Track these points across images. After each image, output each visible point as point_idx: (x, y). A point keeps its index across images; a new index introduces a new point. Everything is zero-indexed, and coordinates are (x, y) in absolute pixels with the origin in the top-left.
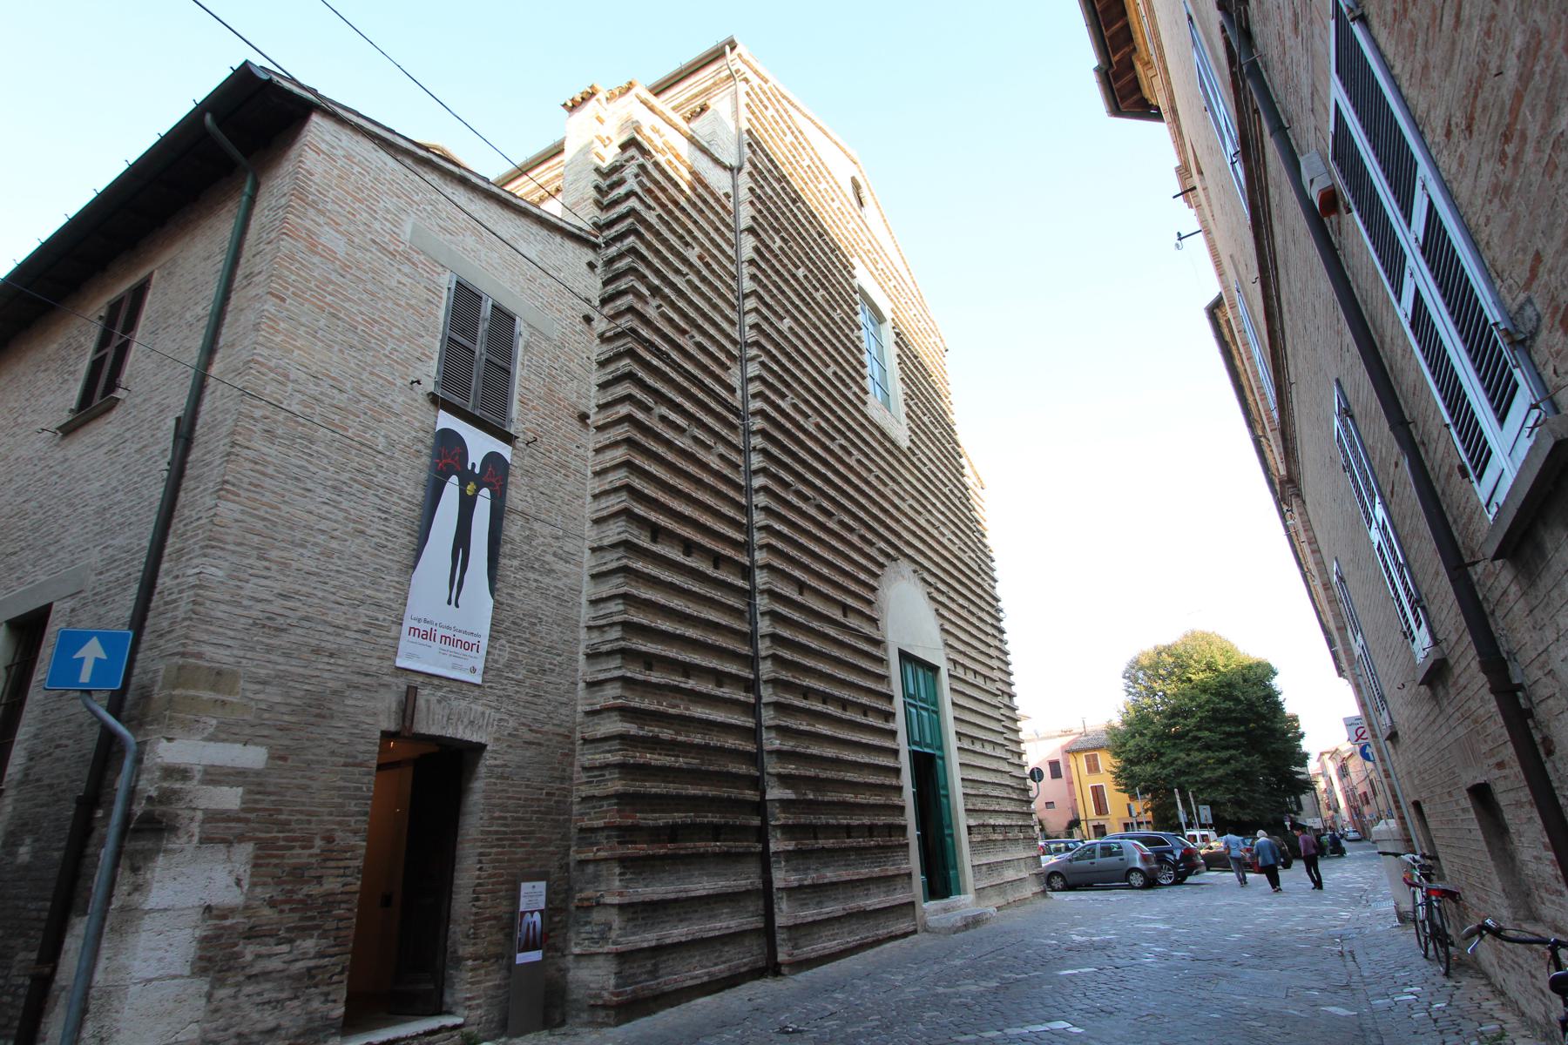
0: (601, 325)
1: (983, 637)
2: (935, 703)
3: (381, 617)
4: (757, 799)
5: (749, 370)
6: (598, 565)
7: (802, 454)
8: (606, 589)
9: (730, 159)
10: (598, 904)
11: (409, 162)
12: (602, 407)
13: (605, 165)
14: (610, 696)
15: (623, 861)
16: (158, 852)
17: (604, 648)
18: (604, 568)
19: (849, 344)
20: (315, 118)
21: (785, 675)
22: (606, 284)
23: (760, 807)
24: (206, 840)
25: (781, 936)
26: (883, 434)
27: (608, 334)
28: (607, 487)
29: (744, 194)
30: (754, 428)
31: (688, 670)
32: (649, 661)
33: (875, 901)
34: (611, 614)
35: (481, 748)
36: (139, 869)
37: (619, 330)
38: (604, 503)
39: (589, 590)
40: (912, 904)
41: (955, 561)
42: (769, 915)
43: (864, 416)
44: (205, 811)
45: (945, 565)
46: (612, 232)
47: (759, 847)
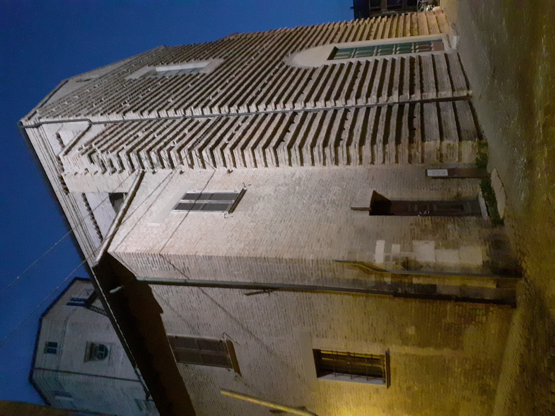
0: (185, 168)
1: (317, 32)
2: (352, 49)
4: (398, 105)
7: (235, 96)
8: (307, 156)
9: (86, 124)
10: (439, 150)
11: (124, 219)
12: (225, 165)
13: (100, 170)
14: (354, 151)
15: (423, 140)
17: (333, 155)
18: (299, 157)
20: (110, 251)
21: (343, 94)
24: (412, 251)
25: (456, 95)
26: (219, 68)
28: (262, 158)
29: (103, 119)
30: (227, 110)
31: (341, 128)
32: (350, 90)
33: (444, 66)
34: (319, 152)
35: (375, 193)
37: (188, 156)
38: (269, 160)
40: (446, 55)
42: (447, 100)
43: (211, 74)
45: (283, 45)
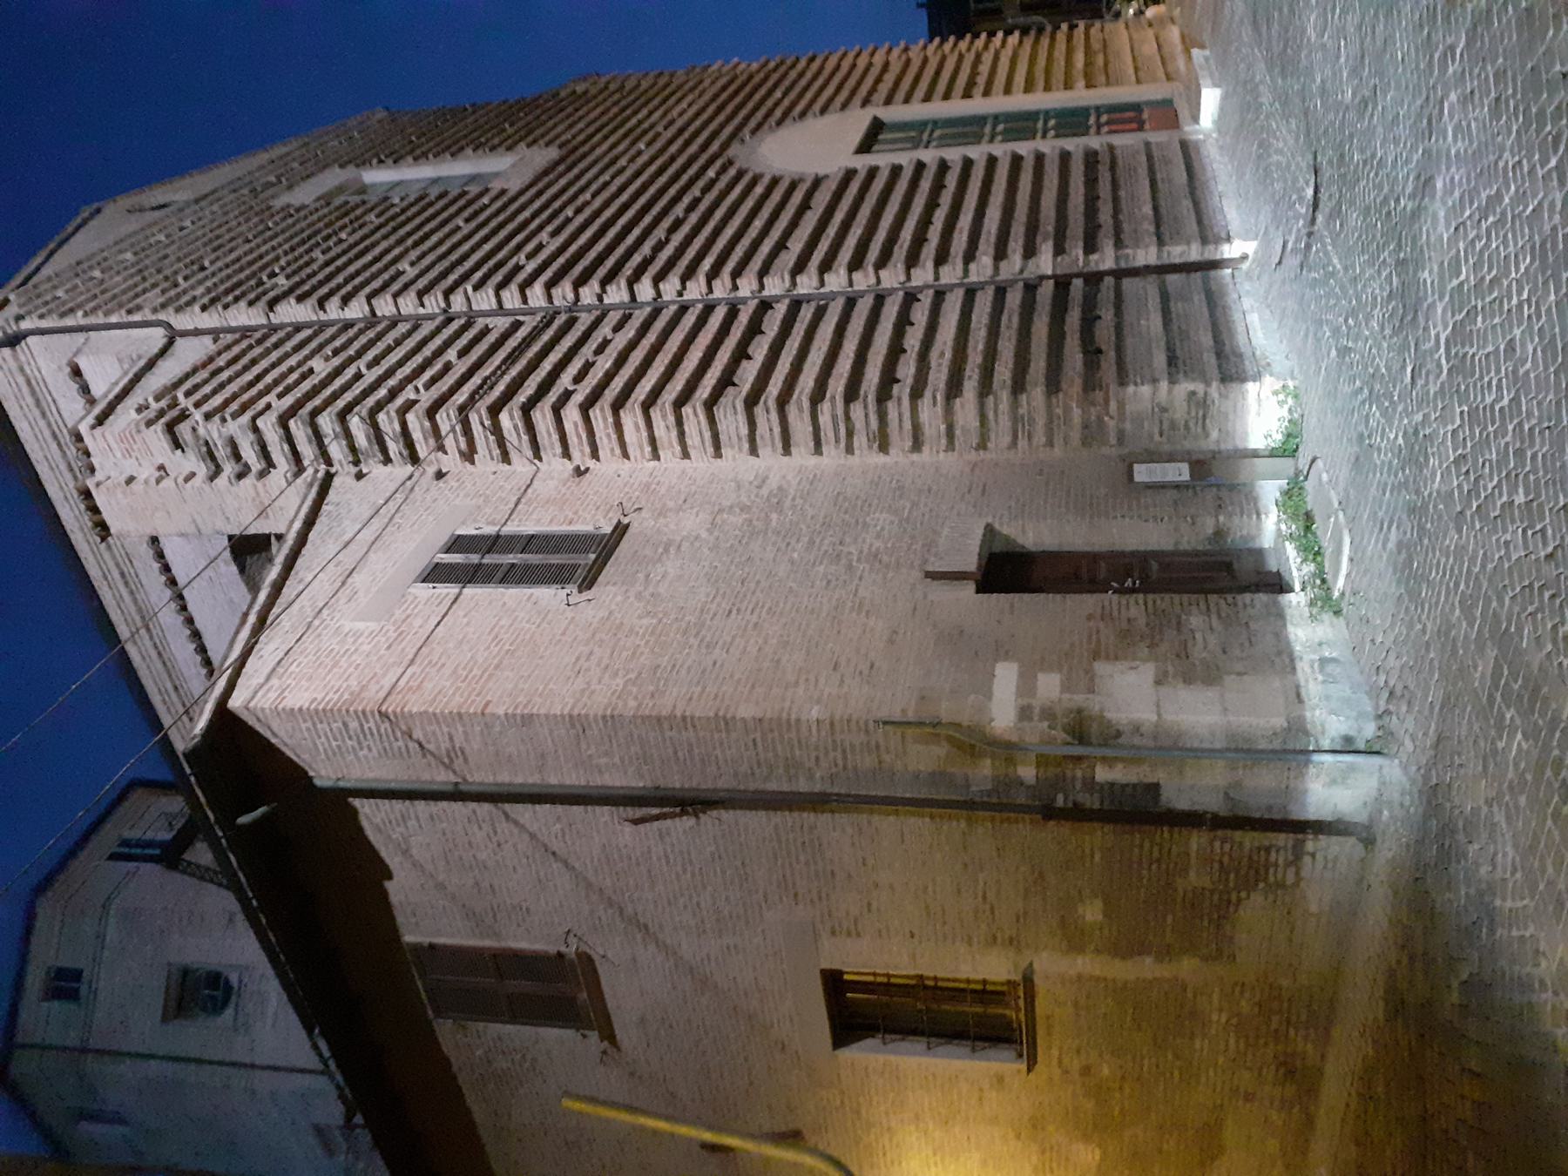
3: (850, 604)
4: (1052, 282)
5: (485, 307)
6: (773, 444)
13: (202, 470)
16: (1103, 717)
19: (367, 274)
20: (235, 703)
21: (900, 252)
22: (387, 460)
23: (1062, 284)
24: (1091, 691)
27: (463, 446)
29: (210, 320)
30: (571, 296)
31: (896, 350)
34: (834, 417)
35: (990, 530)
36: (1118, 731)
37: (458, 428)
38: (693, 439)
39: (802, 456)
41: (685, 178)
43: (521, 193)
44: (1061, 692)
46: (307, 451)
47: (1109, 281)
